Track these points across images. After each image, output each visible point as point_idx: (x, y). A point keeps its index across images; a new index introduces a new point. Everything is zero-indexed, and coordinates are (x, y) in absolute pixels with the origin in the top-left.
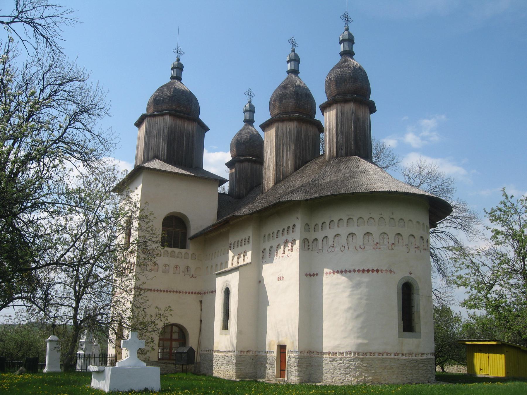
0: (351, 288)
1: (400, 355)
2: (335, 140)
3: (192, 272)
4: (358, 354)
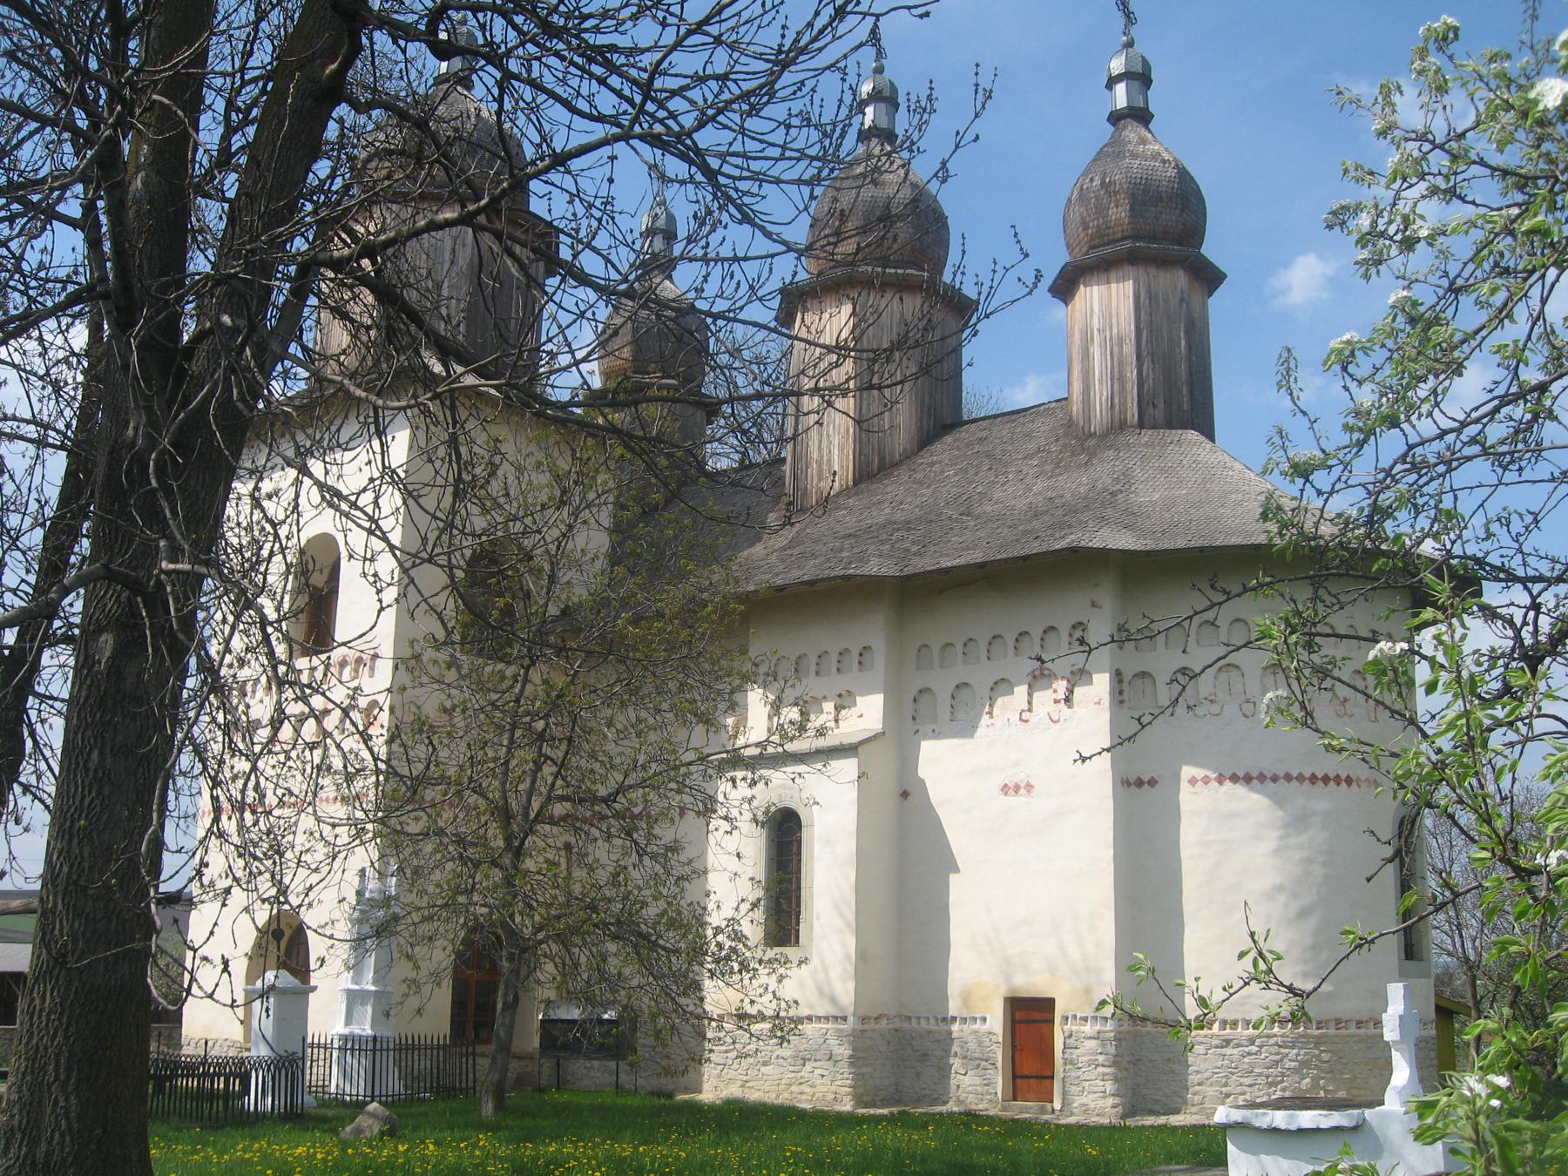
0: (1281, 827)
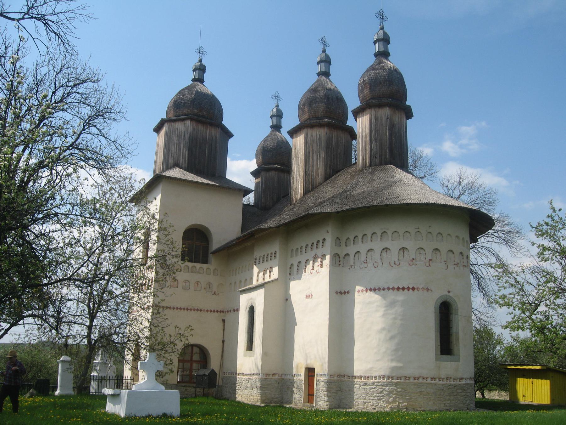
1: (437, 380)
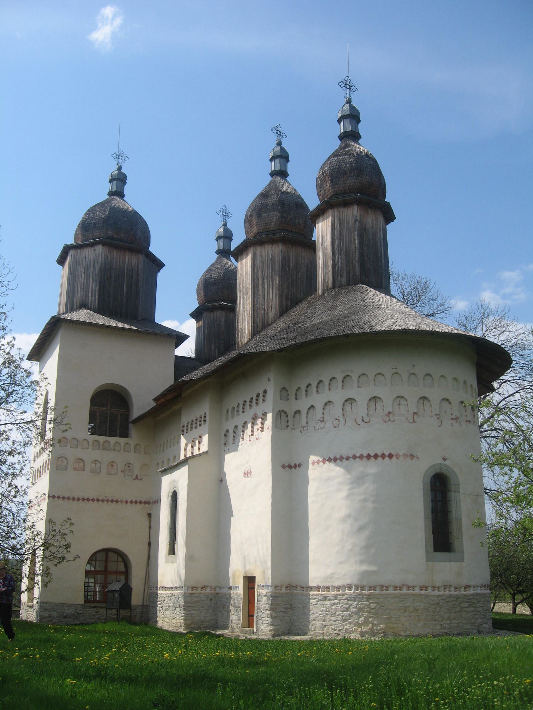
1: (430, 589)
2: (330, 262)
3: (136, 472)
4: (362, 588)
